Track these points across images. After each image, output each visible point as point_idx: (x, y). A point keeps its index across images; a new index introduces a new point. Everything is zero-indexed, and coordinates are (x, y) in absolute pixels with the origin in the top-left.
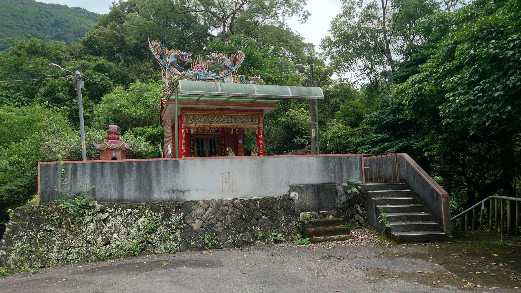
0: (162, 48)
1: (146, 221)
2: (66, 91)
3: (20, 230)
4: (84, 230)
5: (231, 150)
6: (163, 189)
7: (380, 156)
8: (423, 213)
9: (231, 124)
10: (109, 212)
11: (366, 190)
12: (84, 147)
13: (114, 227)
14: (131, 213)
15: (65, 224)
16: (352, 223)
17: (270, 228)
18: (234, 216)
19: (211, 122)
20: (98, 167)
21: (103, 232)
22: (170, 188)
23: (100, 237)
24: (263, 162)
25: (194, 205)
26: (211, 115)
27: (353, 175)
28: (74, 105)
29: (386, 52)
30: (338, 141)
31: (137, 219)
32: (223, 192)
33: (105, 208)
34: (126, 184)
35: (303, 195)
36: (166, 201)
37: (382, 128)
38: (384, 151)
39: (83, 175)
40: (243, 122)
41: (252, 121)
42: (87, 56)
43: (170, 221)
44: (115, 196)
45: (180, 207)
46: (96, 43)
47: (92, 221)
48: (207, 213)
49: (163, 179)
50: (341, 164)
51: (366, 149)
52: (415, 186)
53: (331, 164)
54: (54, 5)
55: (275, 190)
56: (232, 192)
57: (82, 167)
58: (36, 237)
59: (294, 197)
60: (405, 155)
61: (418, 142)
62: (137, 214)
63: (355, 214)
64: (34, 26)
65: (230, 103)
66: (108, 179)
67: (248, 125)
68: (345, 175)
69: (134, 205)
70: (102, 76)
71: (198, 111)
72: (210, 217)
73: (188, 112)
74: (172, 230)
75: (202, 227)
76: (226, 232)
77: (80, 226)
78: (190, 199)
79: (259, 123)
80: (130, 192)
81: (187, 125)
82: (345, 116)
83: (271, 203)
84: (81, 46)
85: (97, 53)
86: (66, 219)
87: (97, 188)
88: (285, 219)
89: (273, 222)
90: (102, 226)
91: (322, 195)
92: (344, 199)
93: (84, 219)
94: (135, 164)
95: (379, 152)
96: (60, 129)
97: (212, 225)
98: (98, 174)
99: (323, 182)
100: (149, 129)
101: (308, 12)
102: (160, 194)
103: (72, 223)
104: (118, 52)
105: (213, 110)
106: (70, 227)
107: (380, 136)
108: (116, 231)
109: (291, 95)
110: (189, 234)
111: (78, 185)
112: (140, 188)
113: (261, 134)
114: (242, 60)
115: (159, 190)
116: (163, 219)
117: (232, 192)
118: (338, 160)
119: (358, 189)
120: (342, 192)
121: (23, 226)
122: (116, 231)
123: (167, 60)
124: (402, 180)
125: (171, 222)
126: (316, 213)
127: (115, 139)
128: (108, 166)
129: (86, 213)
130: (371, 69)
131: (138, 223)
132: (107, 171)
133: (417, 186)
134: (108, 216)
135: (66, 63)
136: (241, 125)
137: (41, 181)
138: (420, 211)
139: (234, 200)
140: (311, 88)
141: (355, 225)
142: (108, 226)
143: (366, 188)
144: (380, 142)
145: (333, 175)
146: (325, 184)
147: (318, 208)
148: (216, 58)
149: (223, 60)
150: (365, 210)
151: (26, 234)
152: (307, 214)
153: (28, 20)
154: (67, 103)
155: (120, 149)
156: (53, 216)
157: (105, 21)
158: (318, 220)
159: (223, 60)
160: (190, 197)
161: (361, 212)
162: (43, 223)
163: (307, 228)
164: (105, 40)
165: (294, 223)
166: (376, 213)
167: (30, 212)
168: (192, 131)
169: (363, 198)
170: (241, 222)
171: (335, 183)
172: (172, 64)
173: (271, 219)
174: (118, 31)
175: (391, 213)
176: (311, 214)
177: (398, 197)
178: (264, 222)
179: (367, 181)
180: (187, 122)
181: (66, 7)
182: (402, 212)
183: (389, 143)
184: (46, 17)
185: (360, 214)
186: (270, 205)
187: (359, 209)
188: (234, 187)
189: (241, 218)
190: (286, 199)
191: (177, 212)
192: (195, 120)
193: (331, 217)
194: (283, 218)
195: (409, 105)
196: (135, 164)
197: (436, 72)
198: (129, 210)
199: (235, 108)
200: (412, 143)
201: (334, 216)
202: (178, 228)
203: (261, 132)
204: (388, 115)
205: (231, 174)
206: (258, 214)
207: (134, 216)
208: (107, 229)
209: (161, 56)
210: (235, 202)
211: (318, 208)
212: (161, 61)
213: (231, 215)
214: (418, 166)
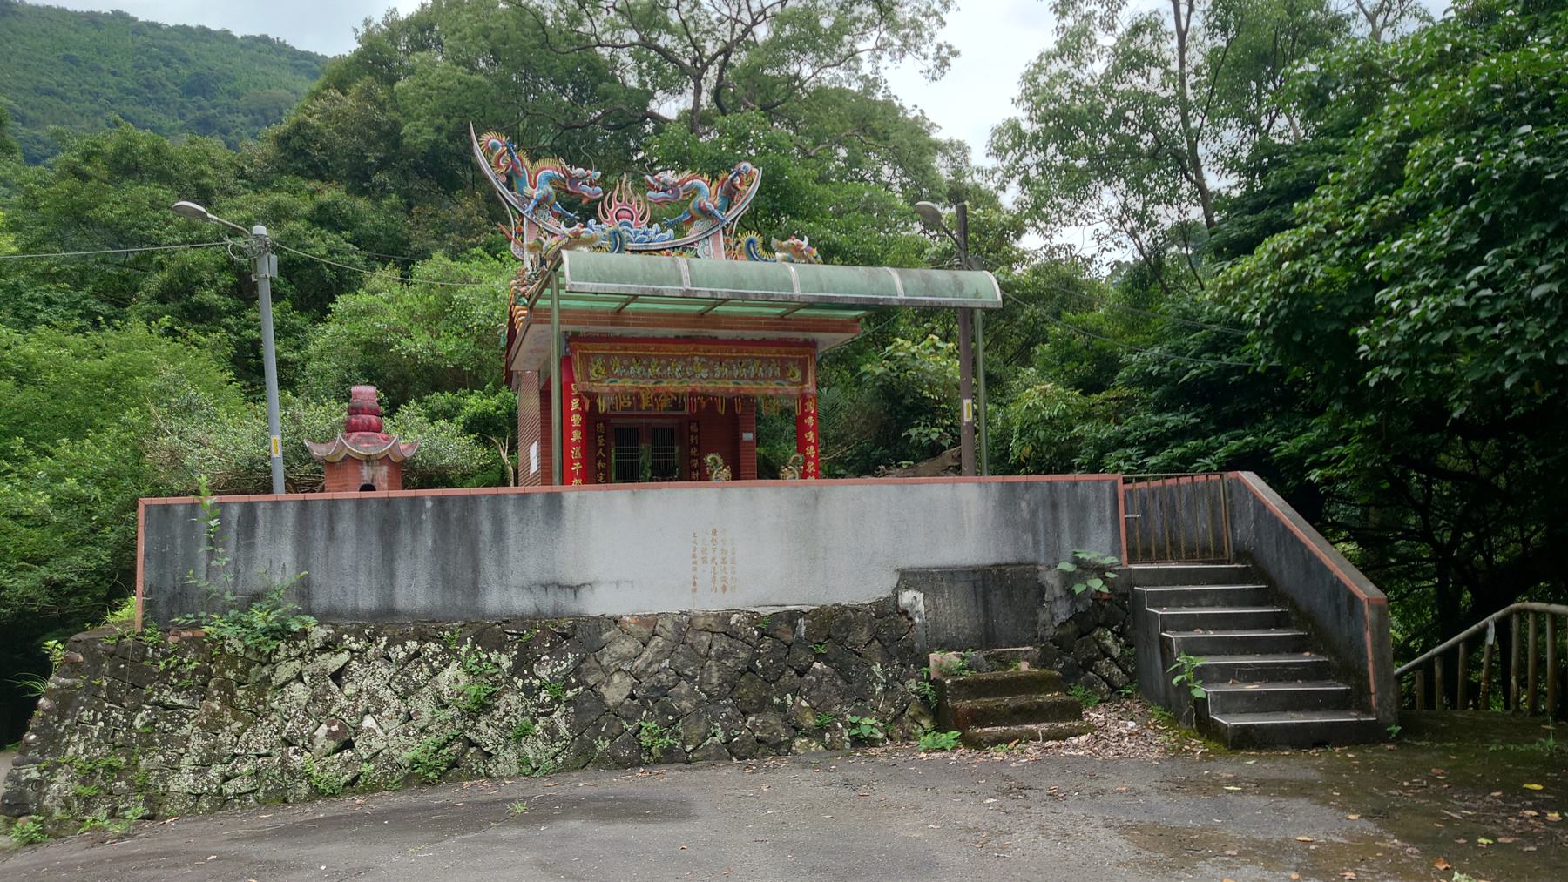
1: (464, 679)
2: (225, 286)
3: (81, 703)
4: (275, 704)
5: (720, 462)
6: (515, 579)
8: (1307, 657)
9: (720, 384)
10: (352, 651)
11: (1132, 585)
12: (277, 453)
13: (364, 696)
14: (417, 654)
15: (219, 686)
16: (1089, 684)
17: (838, 699)
19: (658, 379)
20: (319, 515)
21: (333, 710)
22: (534, 578)
23: (324, 727)
27: (1092, 540)
28: (249, 327)
30: (1042, 434)
31: (435, 672)
32: (694, 590)
33: (339, 639)
34: (402, 567)
35: (940, 601)
36: (522, 618)
38: (1184, 465)
39: (275, 535)
40: (756, 378)
41: (784, 375)
42: (287, 181)
43: (536, 677)
44: (368, 601)
45: (565, 636)
48: (648, 654)
49: (513, 551)
50: (1054, 506)
51: (1128, 459)
53: (1024, 505)
55: (856, 584)
56: (724, 589)
58: (130, 727)
59: (912, 606)
60: (1250, 478)
61: (1286, 439)
63: (1098, 658)
64: (129, 92)
67: (771, 387)
68: (1067, 540)
70: (332, 239)
72: (655, 667)
73: (590, 348)
74: (542, 706)
75: (632, 697)
77: (261, 694)
78: (594, 611)
80: (415, 590)
81: (587, 386)
83: (843, 623)
84: (269, 149)
85: (319, 172)
86: (221, 671)
87: (317, 578)
88: (885, 674)
89: (848, 680)
90: (329, 692)
91: (997, 598)
92: (1062, 612)
93: (274, 671)
94: (429, 504)
95: (1167, 469)
96: (206, 399)
97: (661, 691)
98: (319, 534)
99: (999, 561)
100: (472, 400)
101: (949, 47)
102: (504, 597)
103: (240, 684)
104: (379, 169)
105: (665, 340)
106: (233, 695)
107: (1172, 420)
108: (372, 709)
109: (901, 296)
110: (594, 717)
111: (259, 567)
112: (445, 578)
113: (809, 414)
114: (753, 190)
115: (501, 585)
116: (515, 671)
117: (724, 589)
119: (1105, 580)
120: (1058, 592)
123: (528, 190)
124: (1241, 555)
125: (537, 682)
126: (978, 656)
128: (347, 511)
129: (283, 654)
130: (1141, 216)
131: (437, 683)
132: (346, 526)
133: (1287, 575)
134: (348, 663)
135: (226, 202)
136: (748, 387)
137: (147, 555)
138: (1298, 650)
141: (1098, 691)
142: (347, 692)
143: (1130, 579)
144: (1173, 438)
145: (1029, 538)
146: (1007, 565)
147: (986, 640)
148: (674, 186)
149: (695, 191)
150: (1129, 646)
151: (100, 716)
152: (952, 658)
153: (114, 74)
155: (385, 460)
156: (181, 663)
157: (342, 75)
158: (985, 676)
159: (695, 191)
160: (596, 604)
161: (1116, 651)
162: (151, 683)
163: (953, 700)
164: (342, 132)
165: (912, 685)
167: (112, 649)
168: (602, 406)
169: (1124, 609)
171: (1035, 564)
172: (542, 203)
173: (842, 671)
174: (381, 107)
175: (1208, 654)
176: (963, 659)
177: (1231, 604)
178: (819, 681)
180: (587, 377)
181: (226, 36)
183: (1200, 442)
184: (167, 64)
185: (1112, 658)
187: (1109, 642)
188: (729, 576)
189: (749, 670)
190: (887, 614)
191: (556, 651)
193: (1024, 667)
194: (877, 668)
195: (1264, 325)
196: (429, 504)
198: (413, 645)
200: (1271, 440)
202: (558, 700)
203: (810, 408)
204: (1197, 356)
206: (803, 658)
207: (427, 661)
208: (344, 702)
209: (509, 178)
211: (986, 640)
213: (719, 659)
214: (1291, 510)
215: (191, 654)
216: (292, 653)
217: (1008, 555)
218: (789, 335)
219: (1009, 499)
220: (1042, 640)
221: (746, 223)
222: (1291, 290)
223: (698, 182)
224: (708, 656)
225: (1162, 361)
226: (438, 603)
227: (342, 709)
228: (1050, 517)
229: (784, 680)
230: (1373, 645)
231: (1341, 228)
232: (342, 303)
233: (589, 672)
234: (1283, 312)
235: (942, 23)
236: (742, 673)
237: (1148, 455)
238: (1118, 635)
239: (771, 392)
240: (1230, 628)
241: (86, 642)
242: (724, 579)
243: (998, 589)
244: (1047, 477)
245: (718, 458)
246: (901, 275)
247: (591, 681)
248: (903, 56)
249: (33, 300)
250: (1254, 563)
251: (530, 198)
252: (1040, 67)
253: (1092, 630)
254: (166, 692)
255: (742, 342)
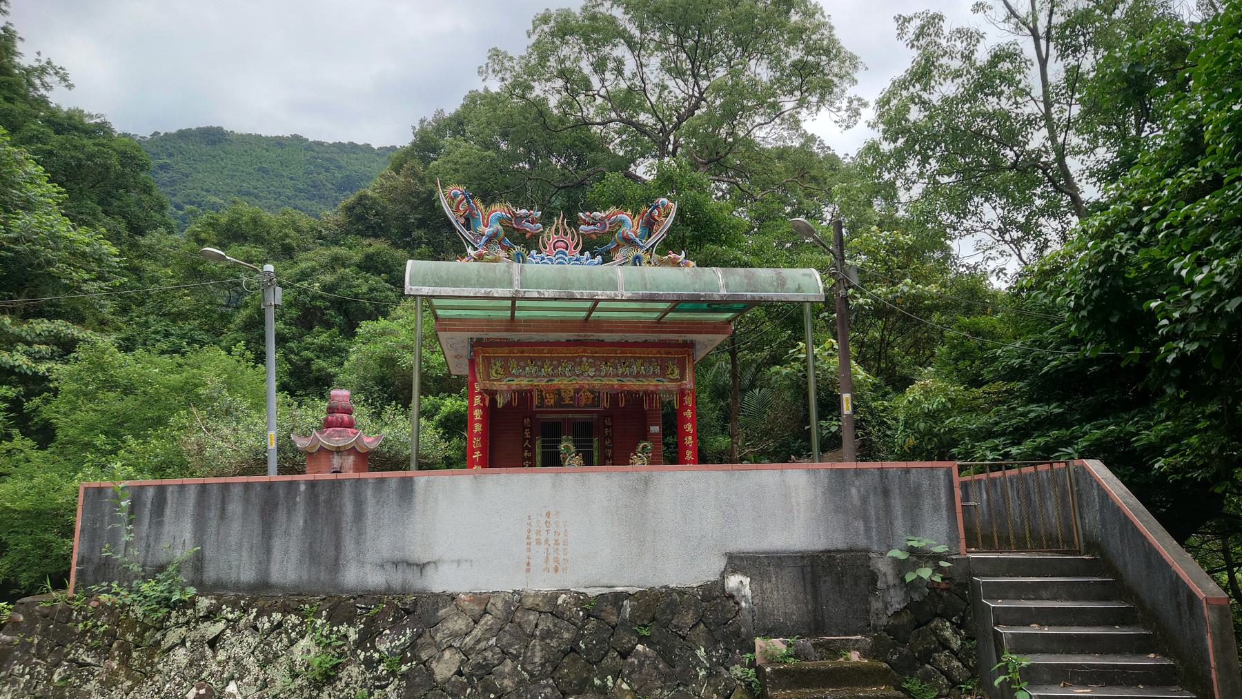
0: (468, 202)
1: (315, 650)
2: (291, 318)
3: (16, 658)
4: (160, 666)
5: (573, 449)
6: (371, 557)
7: (1031, 469)
8: (1151, 659)
9: (606, 381)
10: (228, 620)
11: (971, 574)
12: (272, 446)
13: (231, 663)
14: (280, 625)
15: (120, 647)
16: (926, 678)
17: (659, 683)
18: (554, 643)
19: (550, 377)
20: (215, 494)
21: (204, 675)
22: (386, 555)
23: (194, 690)
24: (646, 482)
25: (444, 607)
26: (551, 359)
27: (927, 529)
28: (307, 349)
29: (1063, 182)
30: (922, 425)
31: (292, 642)
32: (528, 570)
33: (219, 609)
34: (277, 544)
35: (766, 586)
36: (375, 593)
37: (1051, 386)
38: (1046, 454)
39: (178, 515)
40: (638, 376)
41: (664, 373)
42: (350, 239)
43: (377, 651)
44: (248, 575)
45: (408, 612)
46: (372, 209)
47: (183, 643)
48: (478, 631)
49: (370, 531)
50: (886, 493)
51: (994, 449)
52: (1125, 565)
53: (854, 491)
54: (343, 145)
55: (683, 567)
56: (556, 570)
57: (176, 495)
58: (50, 681)
59: (738, 590)
60: (1096, 467)
61: (1148, 428)
62: (294, 627)
63: (936, 650)
64: (301, 191)
65: (600, 325)
66: (236, 526)
67: (651, 384)
68: (900, 525)
69: (292, 601)
70: (374, 280)
71: (516, 349)
72: (483, 645)
73: (491, 352)
74: (378, 679)
75: (459, 673)
76: (526, 691)
77: (151, 657)
78: (437, 588)
79: (683, 377)
80: (287, 568)
81: (488, 385)
82: (957, 360)
83: (668, 605)
84: (341, 217)
85: (374, 231)
86: (123, 634)
87: (209, 553)
88: (709, 659)
89: (671, 664)
90: (203, 657)
91: (826, 586)
92: (897, 601)
93: (164, 635)
94: (303, 488)
95: (1032, 458)
97: (486, 669)
98: (213, 514)
99: (829, 547)
100: (448, 402)
101: (859, 100)
102: (363, 573)
103: (137, 646)
104: (419, 227)
105: (557, 343)
106: (130, 656)
107: (1036, 410)
108: (237, 676)
109: (723, 292)
110: (422, 692)
111: (165, 544)
112: (312, 555)
113: (687, 407)
114: (669, 221)
115: (359, 561)
116: (360, 644)
117: (556, 570)
118: (877, 478)
119: (938, 569)
120: (891, 579)
121: (25, 647)
122: (237, 676)
123: (481, 228)
124: (1091, 546)
125: (376, 655)
126: (806, 643)
127: (342, 424)
128: (237, 492)
129: (173, 620)
130: (1026, 228)
131: (292, 653)
132: (235, 507)
133: (1133, 570)
134: (223, 631)
135: (302, 255)
136: (632, 384)
137: (82, 531)
138: (1143, 651)
139: (556, 595)
140: (787, 272)
141: (936, 686)
142: (219, 658)
143: (970, 568)
144: (1035, 429)
145: (860, 525)
146: (838, 551)
147: (815, 626)
148: (602, 219)
149: (621, 223)
150: (970, 638)
151: (27, 670)
152: (778, 645)
153: (291, 179)
154: (291, 344)
155: (352, 450)
156: (95, 626)
157: (399, 160)
158: (808, 665)
159: (621, 223)
160: (438, 582)
161: (956, 643)
162: (71, 642)
163: (774, 689)
164: (394, 201)
165: (737, 671)
166: (997, 651)
167: (46, 611)
168: (501, 402)
169: (963, 598)
170: (574, 660)
171: (868, 551)
172: (491, 239)
173: (665, 654)
174: (422, 180)
175: (1042, 652)
176: (789, 646)
177: (1074, 598)
178: (641, 664)
179: (971, 541)
180: (488, 377)
181: (367, 148)
182: (1082, 652)
183: (1063, 432)
184: (327, 170)
185: (952, 651)
186: (664, 612)
187: (948, 633)
188: (561, 557)
189: (572, 650)
190: (713, 597)
191: (397, 626)
192: (508, 374)
193: (854, 656)
194: (701, 653)
195: (1078, 308)
196: (303, 488)
197: (1156, 200)
198: (277, 616)
199: (616, 337)
200: (1133, 429)
201: (864, 654)
202: (393, 673)
203: (689, 401)
204: (1057, 348)
205: (553, 519)
206: (626, 640)
207: (287, 632)
208: (214, 668)
209: (467, 220)
210: (560, 601)
211: (815, 626)
212: (466, 233)
213: (543, 639)
214: (1133, 500)
215: (104, 618)
216: (180, 621)
217: (838, 541)
218: (666, 335)
219: (839, 481)
220: (875, 630)
221: (667, 246)
222: (1100, 270)
223: (624, 216)
224: (533, 636)
225: (1024, 355)
226: (305, 578)
227: (211, 674)
228: (881, 504)
229: (607, 661)
230: (1216, 651)
231: (1150, 203)
232: (366, 327)
233: (423, 647)
234: (1096, 293)
235: (854, 82)
236: (566, 653)
237: (1013, 444)
238: (957, 627)
239: (652, 388)
240: (1071, 624)
241: (27, 605)
242: (556, 560)
243: (828, 577)
244: (878, 464)
245: (571, 446)
246: (724, 274)
247: (424, 656)
248: (818, 110)
249: (156, 332)
250: (1102, 554)
251: (482, 235)
252: (892, 93)
253: (930, 621)
254: (81, 650)
255: (625, 344)
